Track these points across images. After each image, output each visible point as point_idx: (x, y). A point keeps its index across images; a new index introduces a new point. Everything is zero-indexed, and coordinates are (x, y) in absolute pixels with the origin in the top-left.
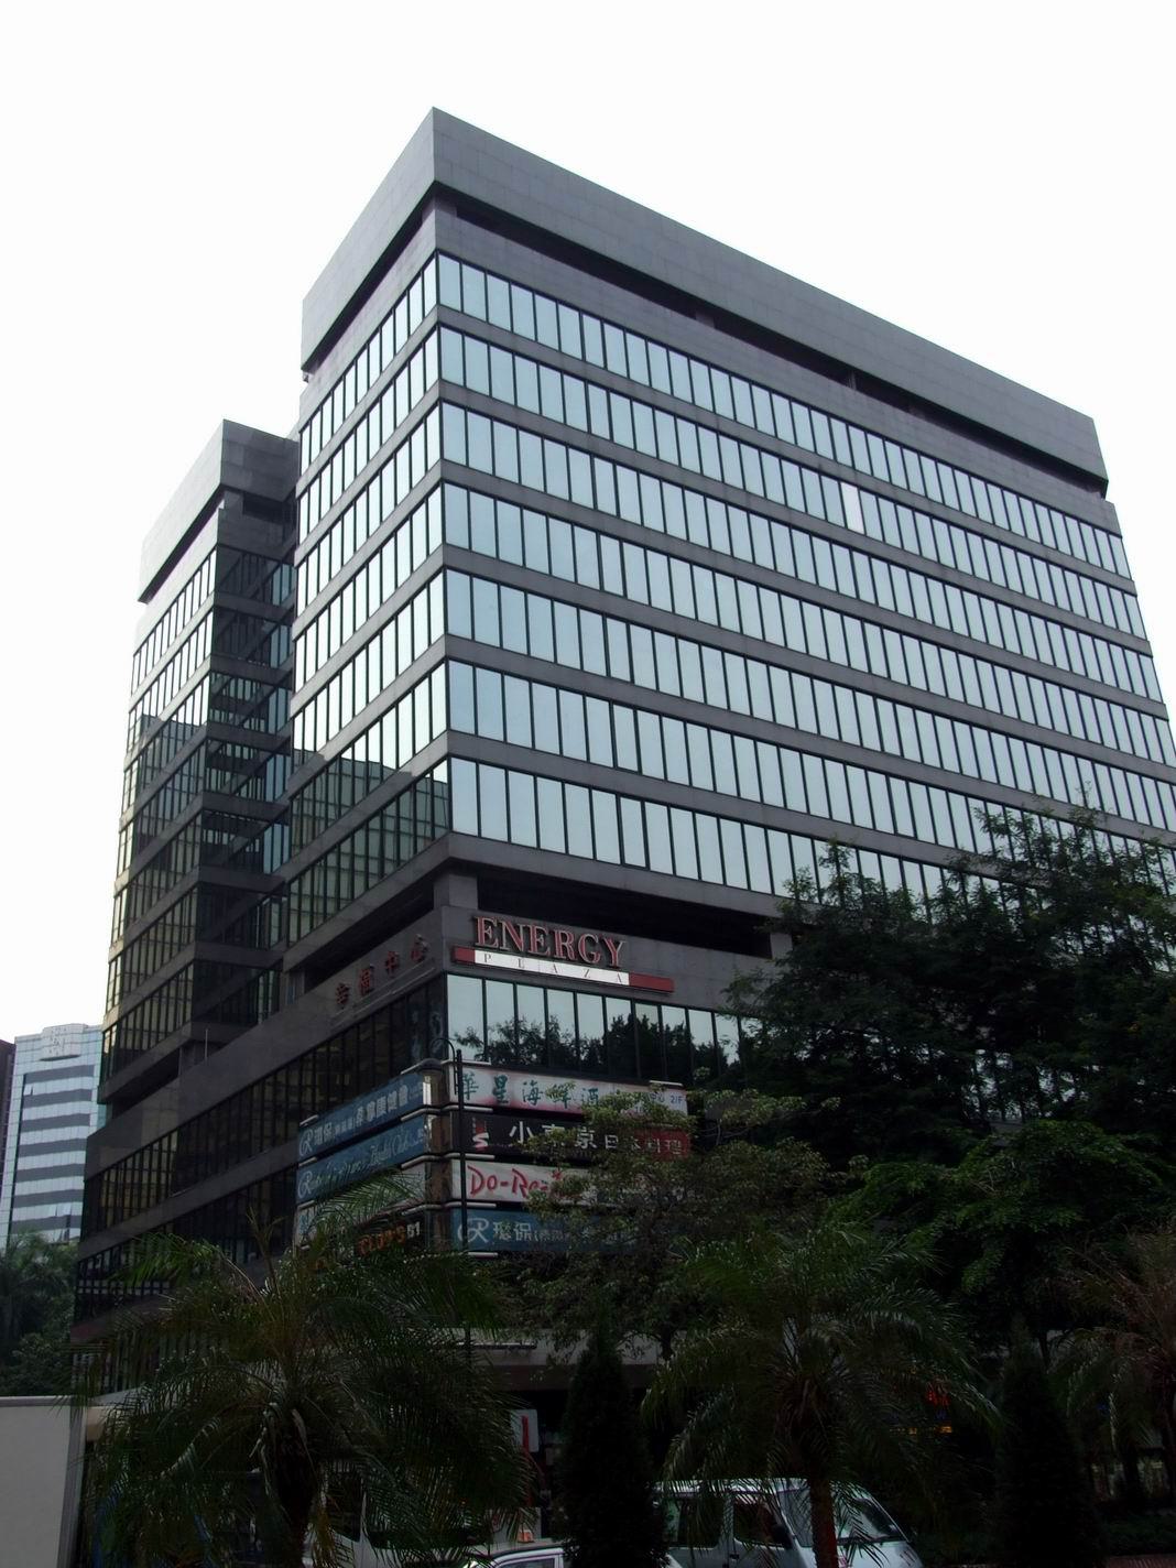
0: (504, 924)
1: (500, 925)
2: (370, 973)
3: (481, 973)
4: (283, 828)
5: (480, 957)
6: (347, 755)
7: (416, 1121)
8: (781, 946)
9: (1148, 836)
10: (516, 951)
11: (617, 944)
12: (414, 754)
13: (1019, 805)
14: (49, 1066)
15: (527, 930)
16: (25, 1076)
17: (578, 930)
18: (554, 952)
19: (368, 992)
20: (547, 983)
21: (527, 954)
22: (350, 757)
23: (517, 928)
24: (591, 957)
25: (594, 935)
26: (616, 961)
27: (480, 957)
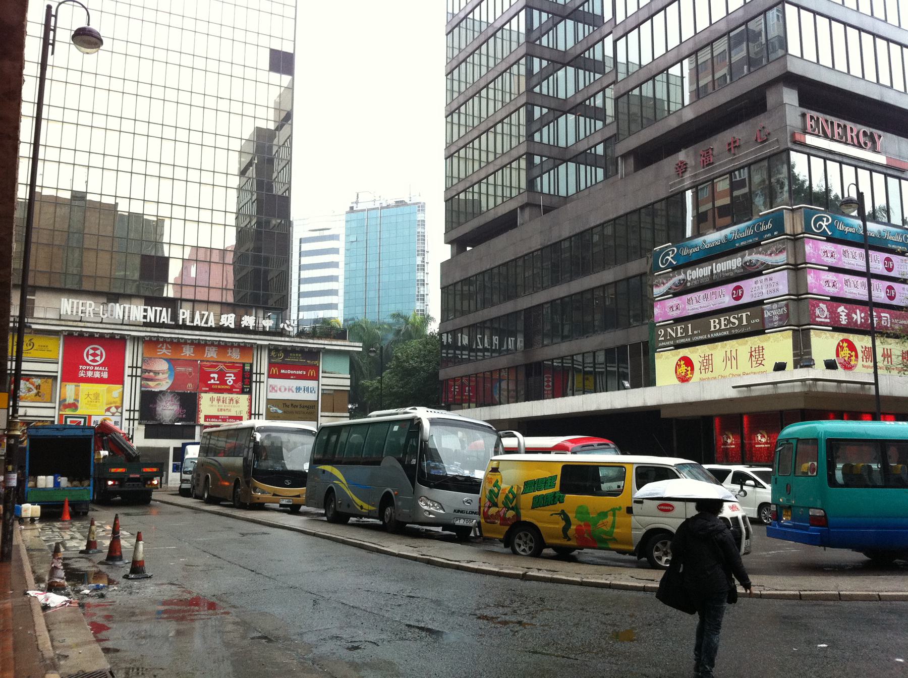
0: (820, 119)
1: (818, 118)
2: (711, 152)
3: (808, 151)
4: (585, 73)
5: (810, 140)
6: (595, 28)
7: (768, 246)
8: (203, 312)
9: (555, 152)
10: (826, 136)
11: (880, 137)
12: (626, 17)
13: (539, 7)
14: (317, 234)
15: (832, 123)
16: (301, 239)
17: (859, 126)
18: (847, 139)
19: (708, 165)
20: (842, 160)
21: (832, 139)
22: (508, 28)
23: (827, 121)
24: (865, 144)
25: (868, 130)
26: (879, 148)
27: (810, 140)
